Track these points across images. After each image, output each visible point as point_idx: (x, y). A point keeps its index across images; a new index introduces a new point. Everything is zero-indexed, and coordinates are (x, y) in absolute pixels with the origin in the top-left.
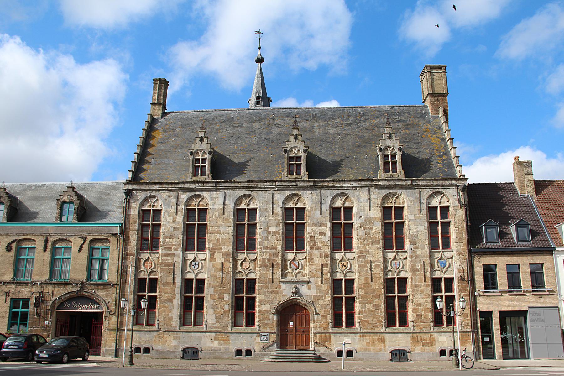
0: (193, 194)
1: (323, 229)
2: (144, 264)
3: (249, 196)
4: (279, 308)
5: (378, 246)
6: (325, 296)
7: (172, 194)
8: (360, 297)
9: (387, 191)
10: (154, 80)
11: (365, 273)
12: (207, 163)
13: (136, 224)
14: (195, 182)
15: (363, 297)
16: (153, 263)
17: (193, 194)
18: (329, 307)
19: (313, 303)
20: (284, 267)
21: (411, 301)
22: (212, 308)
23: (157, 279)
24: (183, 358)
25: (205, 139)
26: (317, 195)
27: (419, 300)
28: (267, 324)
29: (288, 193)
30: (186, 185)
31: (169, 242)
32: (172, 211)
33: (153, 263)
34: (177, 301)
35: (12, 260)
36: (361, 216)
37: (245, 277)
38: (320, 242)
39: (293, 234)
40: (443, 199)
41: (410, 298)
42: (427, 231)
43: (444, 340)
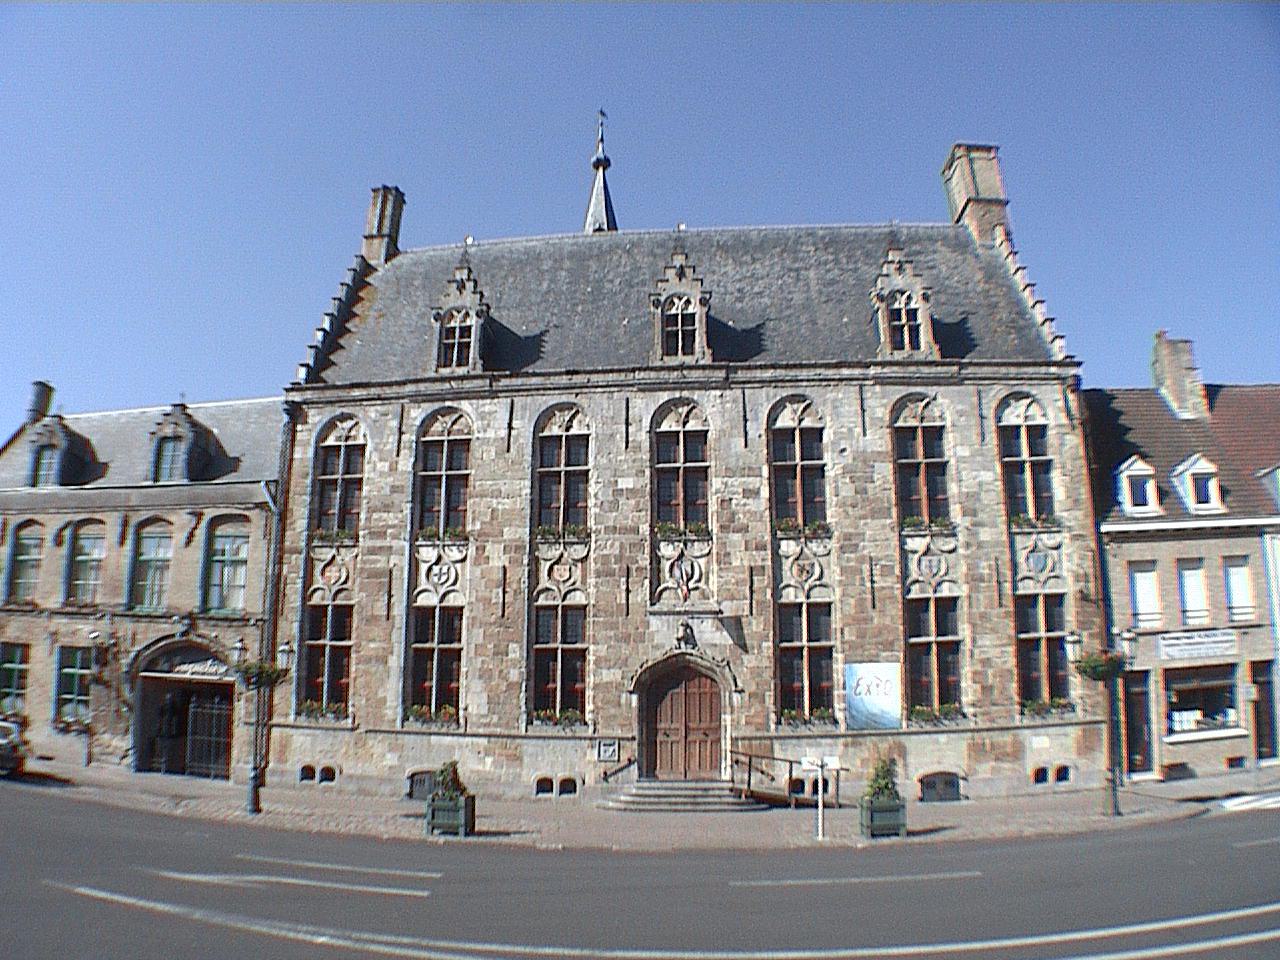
0: (437, 405)
1: (753, 482)
2: (323, 574)
3: (570, 406)
4: (643, 678)
5: (888, 521)
6: (760, 646)
7: (390, 407)
8: (847, 647)
9: (904, 390)
10: (374, 191)
11: (858, 588)
12: (473, 339)
13: (308, 481)
14: (443, 379)
15: (852, 646)
16: (341, 572)
17: (437, 405)
18: (768, 674)
19: (728, 664)
20: (656, 578)
21: (968, 653)
22: (480, 677)
23: (352, 607)
24: (410, 795)
25: (470, 285)
26: (735, 401)
27: (987, 650)
28: (615, 716)
29: (665, 396)
30: (422, 387)
31: (380, 519)
32: (389, 447)
33: (341, 572)
34: (396, 661)
35: (63, 562)
36: (843, 450)
37: (558, 602)
38: (744, 514)
39: (677, 486)
40: (1031, 408)
41: (966, 647)
42: (999, 483)
43: (1045, 745)
